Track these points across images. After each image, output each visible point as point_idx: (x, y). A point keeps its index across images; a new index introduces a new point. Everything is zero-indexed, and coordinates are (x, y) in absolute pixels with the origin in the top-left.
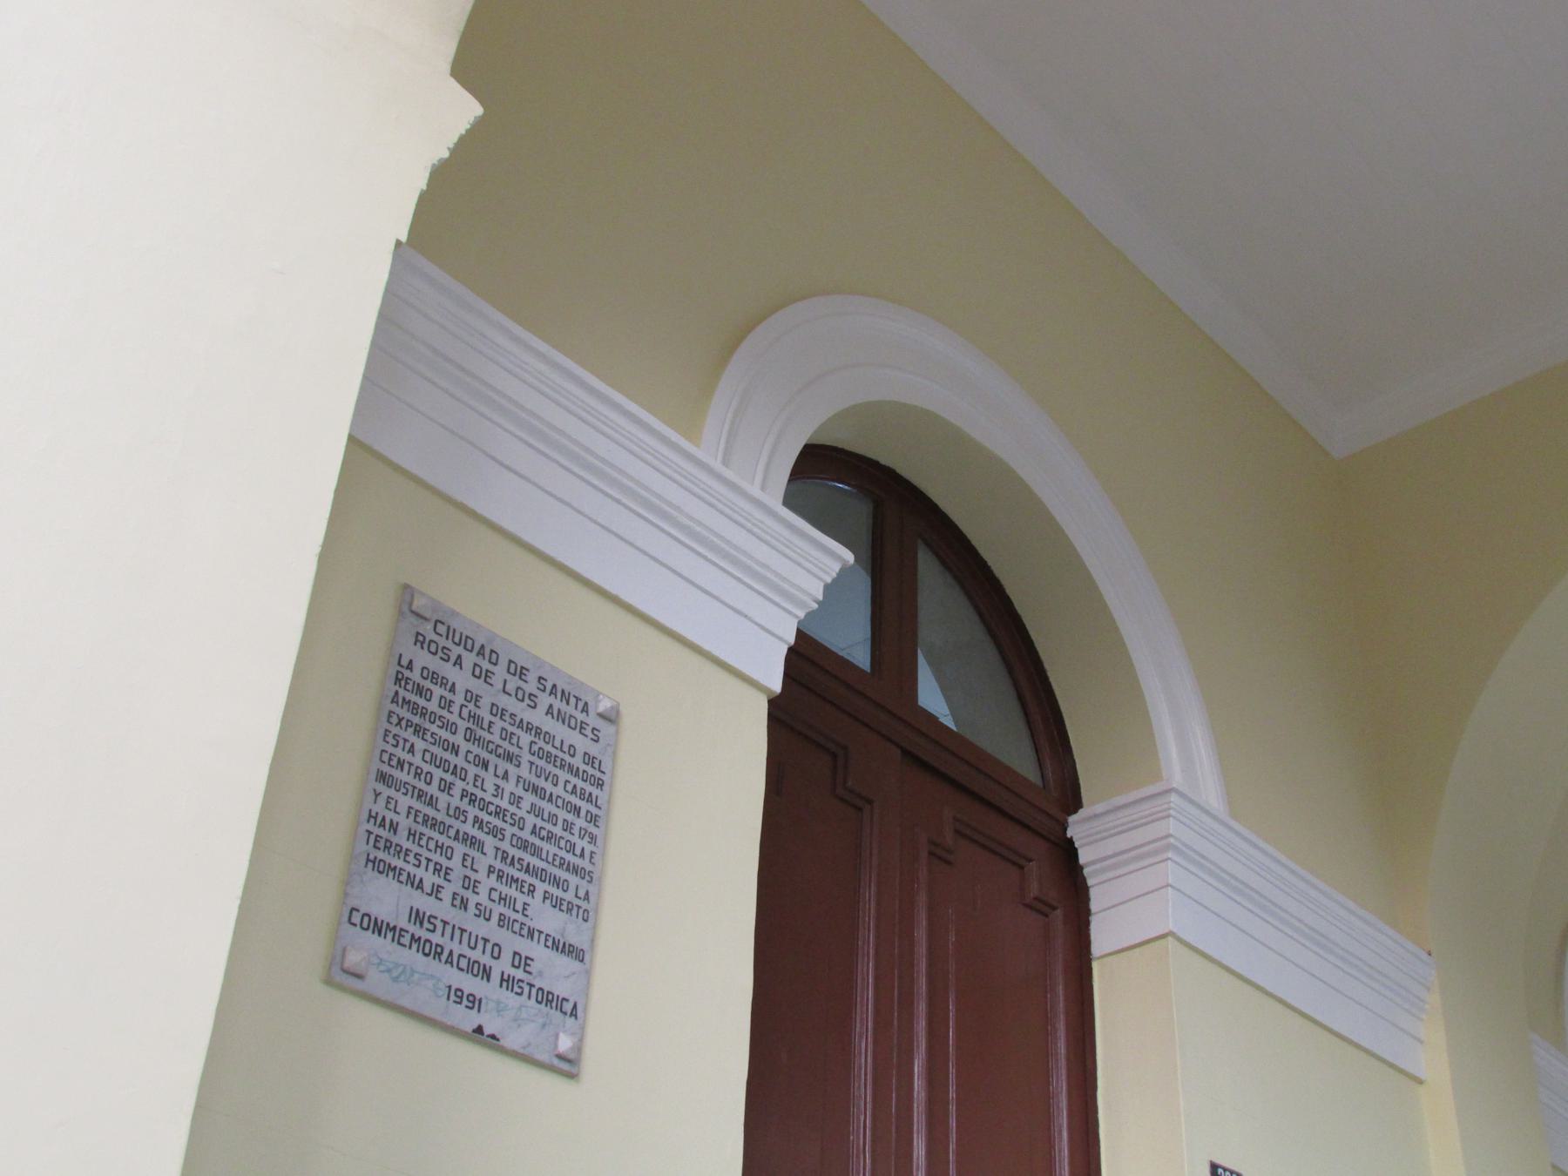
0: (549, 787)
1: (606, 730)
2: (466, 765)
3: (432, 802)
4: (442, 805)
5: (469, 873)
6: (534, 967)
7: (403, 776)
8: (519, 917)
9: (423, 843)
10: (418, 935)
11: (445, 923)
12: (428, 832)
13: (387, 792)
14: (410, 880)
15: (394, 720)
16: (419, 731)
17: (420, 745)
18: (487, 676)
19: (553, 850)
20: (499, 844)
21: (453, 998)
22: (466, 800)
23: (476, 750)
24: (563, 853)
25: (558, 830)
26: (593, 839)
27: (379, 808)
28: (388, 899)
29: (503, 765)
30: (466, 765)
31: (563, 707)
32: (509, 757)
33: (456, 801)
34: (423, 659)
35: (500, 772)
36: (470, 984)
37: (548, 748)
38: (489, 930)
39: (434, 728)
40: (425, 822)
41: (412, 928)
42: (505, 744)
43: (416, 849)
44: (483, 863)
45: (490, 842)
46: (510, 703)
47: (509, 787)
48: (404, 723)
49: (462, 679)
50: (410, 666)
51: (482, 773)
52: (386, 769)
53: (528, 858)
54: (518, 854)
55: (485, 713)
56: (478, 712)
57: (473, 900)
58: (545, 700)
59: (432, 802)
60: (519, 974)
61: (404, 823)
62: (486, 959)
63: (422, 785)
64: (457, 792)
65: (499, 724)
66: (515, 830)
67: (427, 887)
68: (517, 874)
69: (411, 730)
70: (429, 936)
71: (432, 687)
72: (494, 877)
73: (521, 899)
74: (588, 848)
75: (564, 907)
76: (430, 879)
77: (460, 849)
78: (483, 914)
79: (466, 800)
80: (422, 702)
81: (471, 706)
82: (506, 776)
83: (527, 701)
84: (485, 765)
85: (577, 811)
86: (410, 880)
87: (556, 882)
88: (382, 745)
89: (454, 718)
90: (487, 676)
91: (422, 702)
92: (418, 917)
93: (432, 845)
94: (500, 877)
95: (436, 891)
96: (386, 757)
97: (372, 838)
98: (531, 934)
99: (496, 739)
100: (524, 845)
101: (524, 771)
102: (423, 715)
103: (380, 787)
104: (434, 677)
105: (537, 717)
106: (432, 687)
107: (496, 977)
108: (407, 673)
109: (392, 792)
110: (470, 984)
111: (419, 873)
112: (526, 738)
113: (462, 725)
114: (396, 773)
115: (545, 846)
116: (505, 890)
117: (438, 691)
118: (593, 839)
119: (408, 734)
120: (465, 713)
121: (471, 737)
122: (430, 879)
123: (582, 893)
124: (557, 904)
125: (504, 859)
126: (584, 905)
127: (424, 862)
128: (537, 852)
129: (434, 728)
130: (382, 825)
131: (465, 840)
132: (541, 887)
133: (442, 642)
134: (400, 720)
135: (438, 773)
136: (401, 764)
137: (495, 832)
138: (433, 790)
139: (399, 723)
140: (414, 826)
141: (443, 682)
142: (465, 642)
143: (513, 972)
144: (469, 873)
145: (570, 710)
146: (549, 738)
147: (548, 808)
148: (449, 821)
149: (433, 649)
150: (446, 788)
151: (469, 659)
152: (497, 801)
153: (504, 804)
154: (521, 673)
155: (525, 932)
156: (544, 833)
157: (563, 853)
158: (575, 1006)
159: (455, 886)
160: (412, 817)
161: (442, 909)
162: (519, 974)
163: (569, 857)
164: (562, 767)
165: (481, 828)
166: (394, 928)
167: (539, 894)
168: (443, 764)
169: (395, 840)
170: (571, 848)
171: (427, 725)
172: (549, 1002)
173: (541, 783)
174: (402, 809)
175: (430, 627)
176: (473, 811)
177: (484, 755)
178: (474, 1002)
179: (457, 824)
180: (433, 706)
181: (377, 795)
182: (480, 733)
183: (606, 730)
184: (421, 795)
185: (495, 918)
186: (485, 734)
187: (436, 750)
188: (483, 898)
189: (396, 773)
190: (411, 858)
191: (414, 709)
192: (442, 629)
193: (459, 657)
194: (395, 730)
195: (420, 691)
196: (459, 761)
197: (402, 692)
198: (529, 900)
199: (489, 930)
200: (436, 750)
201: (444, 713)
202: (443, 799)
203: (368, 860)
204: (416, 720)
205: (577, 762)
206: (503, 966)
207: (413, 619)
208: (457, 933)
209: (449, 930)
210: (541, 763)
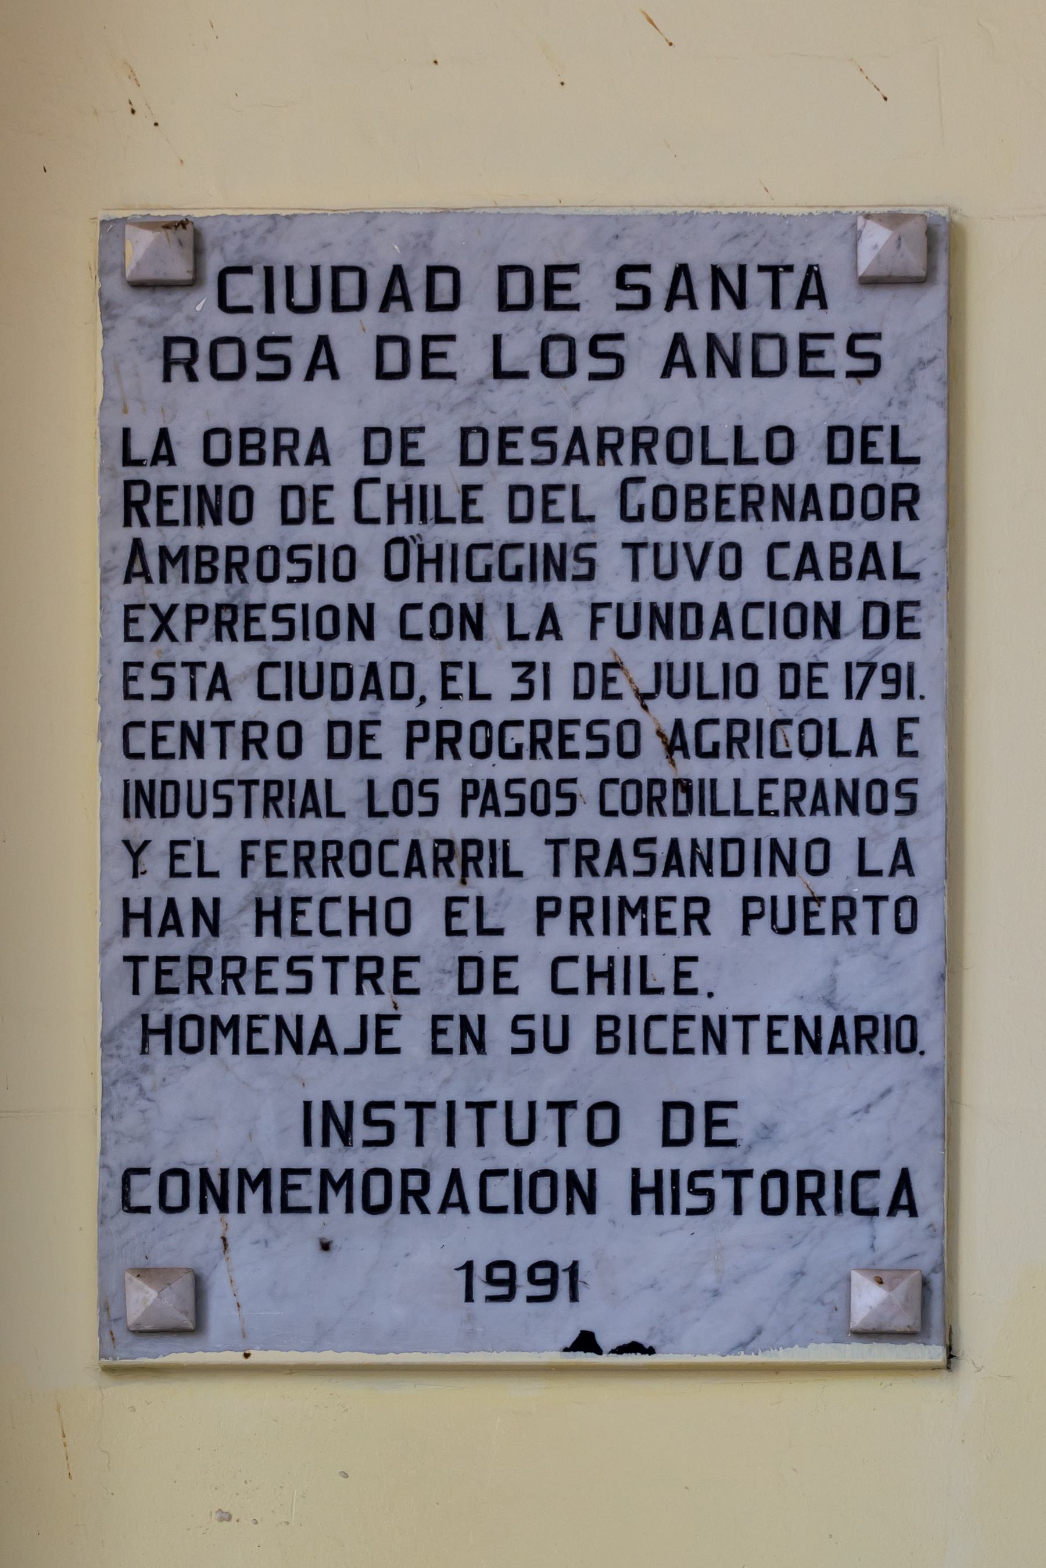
0: (710, 592)
1: (903, 322)
2: (407, 652)
3: (314, 800)
4: (348, 794)
5: (473, 944)
6: (740, 1125)
7: (209, 768)
8: (669, 1004)
9: (309, 921)
10: (354, 1172)
11: (420, 1107)
12: (317, 887)
13: (160, 832)
14: (289, 1035)
15: (148, 623)
16: (230, 621)
17: (241, 658)
18: (430, 359)
19: (750, 769)
20: (555, 827)
21: (481, 1289)
22: (607, 629)
23: (429, 592)
24: (797, 767)
25: (766, 706)
26: (900, 680)
27: (155, 884)
28: (239, 1109)
29: (529, 598)
30: (407, 652)
31: (726, 321)
32: (552, 564)
33: (393, 764)
34: (200, 406)
35: (528, 621)
36: (525, 1239)
37: (696, 472)
38: (579, 1072)
39: (279, 592)
40: (303, 861)
41: (316, 1158)
42: (536, 532)
43: (289, 946)
44: (511, 903)
45: (527, 837)
46: (530, 402)
47: (561, 656)
48: (178, 623)
49: (342, 408)
50: (164, 449)
51: (464, 649)
52: (149, 770)
53: (665, 828)
54: (627, 829)
55: (443, 472)
56: (418, 477)
57: (497, 1012)
58: (649, 335)
59: (314, 800)
60: (695, 1157)
61: (234, 892)
62: (577, 1156)
63: (275, 768)
64: (389, 739)
65: (494, 480)
66: (613, 766)
67: (346, 1034)
68: (633, 889)
69: (203, 631)
70: (378, 1158)
71: (246, 475)
72: (558, 926)
73: (660, 953)
74: (884, 715)
75: (824, 920)
76: (345, 1010)
77: (428, 893)
78: (539, 1038)
79: (425, 750)
80: (222, 535)
81: (392, 472)
82: (550, 623)
83: (587, 364)
84: (473, 623)
85: (828, 621)
86: (289, 1035)
87: (782, 857)
88: (125, 711)
89: (343, 530)
90: (430, 359)
91: (222, 535)
92: (331, 1122)
93: (338, 917)
94: (579, 920)
95: (376, 1036)
96: (141, 741)
97: (148, 972)
98: (715, 1035)
99: (498, 528)
100: (650, 797)
101: (615, 584)
102: (235, 569)
103: (145, 827)
104: (250, 444)
105: (644, 397)
106: (246, 475)
107: (613, 1190)
108: (157, 475)
109: (182, 826)
110: (525, 1239)
111: (315, 1005)
112: (598, 482)
113: (370, 542)
114: (188, 770)
115: (724, 770)
116: (602, 947)
117: (267, 480)
118: (900, 680)
119: (205, 646)
120: (375, 500)
121: (406, 561)
122: (345, 1010)
123: (880, 857)
124: (798, 919)
125: (585, 863)
126: (894, 887)
127: (321, 972)
128: (695, 797)
129: (279, 592)
130: (172, 922)
131: (442, 862)
132: (725, 894)
133: (251, 328)
134: (164, 619)
135: (315, 716)
136: (192, 739)
137: (536, 801)
138: (314, 764)
139: (164, 627)
140: (269, 890)
141: (283, 444)
142: (336, 287)
143: (671, 1159)
144: (473, 944)
145: (759, 316)
146: (687, 442)
147: (712, 653)
148: (375, 831)
149: (228, 361)
150: (353, 741)
151: (353, 336)
152: (534, 708)
153: (560, 705)
154: (552, 286)
155: (693, 1038)
156: (715, 734)
157: (797, 767)
158: (905, 1180)
159: (437, 992)
160: (257, 869)
161: (411, 1072)
162: (695, 1157)
163: (825, 769)
164: (750, 509)
165: (490, 807)
166: (265, 1175)
167: (725, 916)
168: (334, 680)
169: (217, 949)
170: (825, 739)
171: (256, 592)
172: (809, 1200)
173: (683, 589)
174: (223, 854)
175: (205, 300)
176: (451, 774)
177: (463, 593)
178: (555, 1280)
179: (405, 829)
180: (265, 529)
181: (136, 852)
182: (435, 535)
183: (903, 322)
184: (274, 796)
185: (583, 1035)
186: (463, 535)
187: (301, 650)
188: (533, 993)
189: (188, 770)
190: (279, 977)
191: (201, 564)
192: (246, 289)
193: (323, 342)
194: (151, 653)
195: (209, 505)
196: (385, 647)
197: (153, 538)
198: (693, 944)
199: (579, 1072)
200: (301, 650)
201: (308, 532)
202: (348, 778)
203: (147, 1032)
204: (217, 593)
205: (810, 469)
206: (642, 1148)
207: (145, 307)
208: (466, 1120)
209: (436, 1122)
210: (677, 530)
